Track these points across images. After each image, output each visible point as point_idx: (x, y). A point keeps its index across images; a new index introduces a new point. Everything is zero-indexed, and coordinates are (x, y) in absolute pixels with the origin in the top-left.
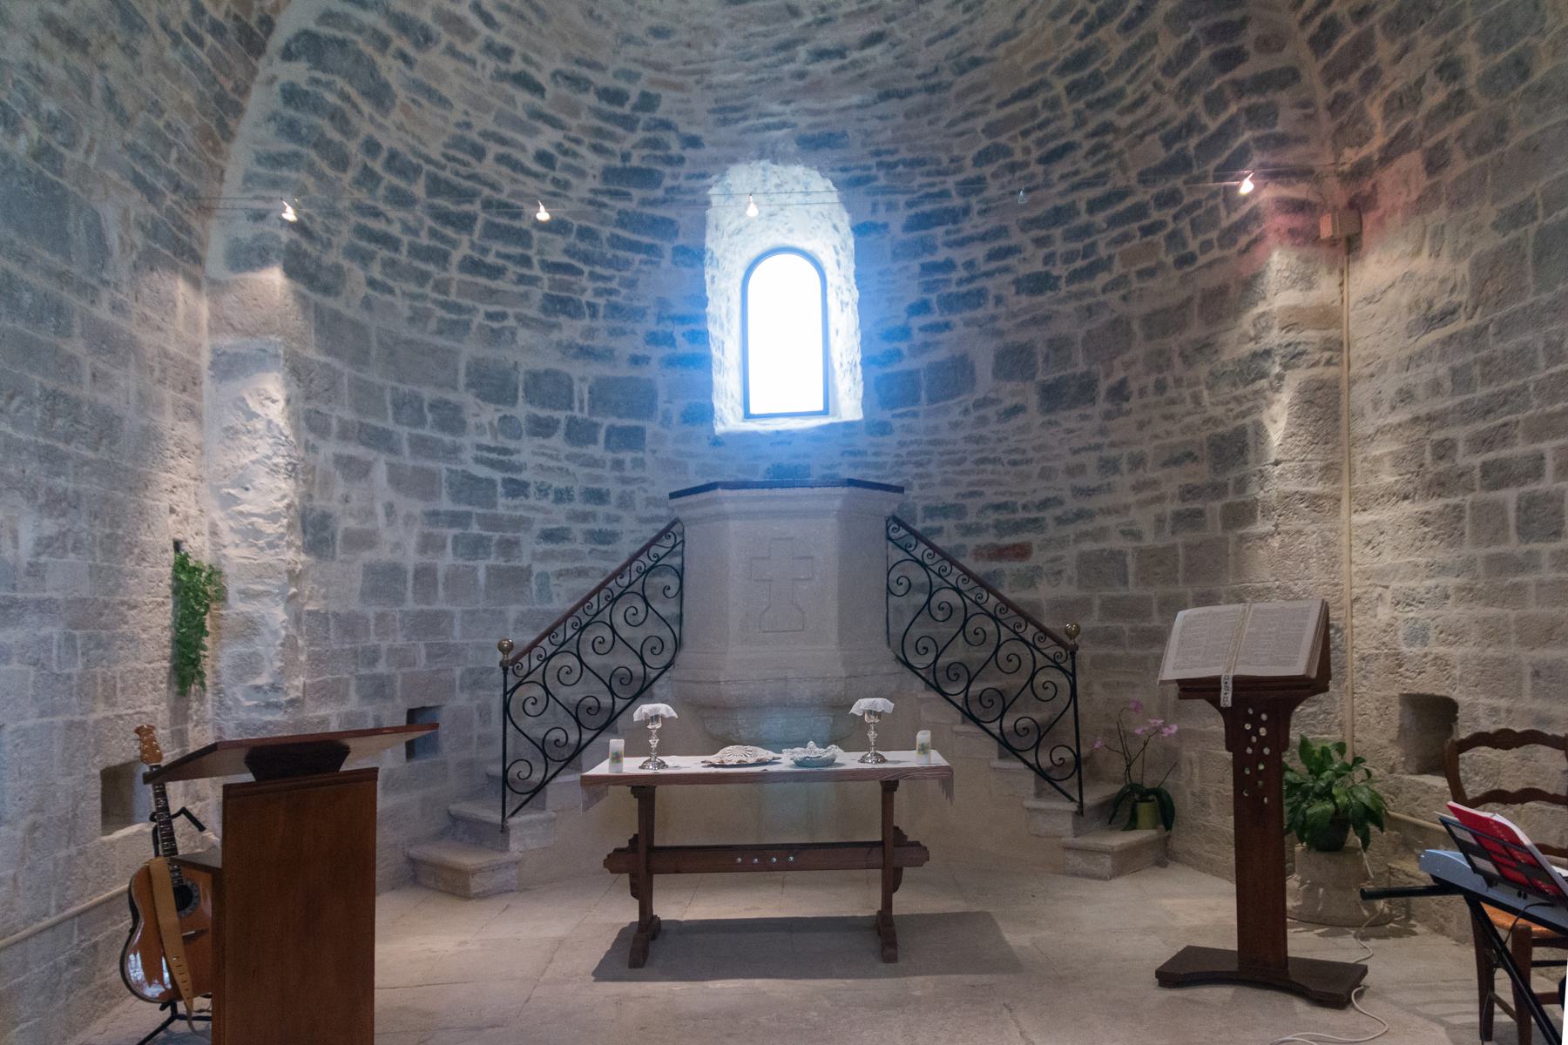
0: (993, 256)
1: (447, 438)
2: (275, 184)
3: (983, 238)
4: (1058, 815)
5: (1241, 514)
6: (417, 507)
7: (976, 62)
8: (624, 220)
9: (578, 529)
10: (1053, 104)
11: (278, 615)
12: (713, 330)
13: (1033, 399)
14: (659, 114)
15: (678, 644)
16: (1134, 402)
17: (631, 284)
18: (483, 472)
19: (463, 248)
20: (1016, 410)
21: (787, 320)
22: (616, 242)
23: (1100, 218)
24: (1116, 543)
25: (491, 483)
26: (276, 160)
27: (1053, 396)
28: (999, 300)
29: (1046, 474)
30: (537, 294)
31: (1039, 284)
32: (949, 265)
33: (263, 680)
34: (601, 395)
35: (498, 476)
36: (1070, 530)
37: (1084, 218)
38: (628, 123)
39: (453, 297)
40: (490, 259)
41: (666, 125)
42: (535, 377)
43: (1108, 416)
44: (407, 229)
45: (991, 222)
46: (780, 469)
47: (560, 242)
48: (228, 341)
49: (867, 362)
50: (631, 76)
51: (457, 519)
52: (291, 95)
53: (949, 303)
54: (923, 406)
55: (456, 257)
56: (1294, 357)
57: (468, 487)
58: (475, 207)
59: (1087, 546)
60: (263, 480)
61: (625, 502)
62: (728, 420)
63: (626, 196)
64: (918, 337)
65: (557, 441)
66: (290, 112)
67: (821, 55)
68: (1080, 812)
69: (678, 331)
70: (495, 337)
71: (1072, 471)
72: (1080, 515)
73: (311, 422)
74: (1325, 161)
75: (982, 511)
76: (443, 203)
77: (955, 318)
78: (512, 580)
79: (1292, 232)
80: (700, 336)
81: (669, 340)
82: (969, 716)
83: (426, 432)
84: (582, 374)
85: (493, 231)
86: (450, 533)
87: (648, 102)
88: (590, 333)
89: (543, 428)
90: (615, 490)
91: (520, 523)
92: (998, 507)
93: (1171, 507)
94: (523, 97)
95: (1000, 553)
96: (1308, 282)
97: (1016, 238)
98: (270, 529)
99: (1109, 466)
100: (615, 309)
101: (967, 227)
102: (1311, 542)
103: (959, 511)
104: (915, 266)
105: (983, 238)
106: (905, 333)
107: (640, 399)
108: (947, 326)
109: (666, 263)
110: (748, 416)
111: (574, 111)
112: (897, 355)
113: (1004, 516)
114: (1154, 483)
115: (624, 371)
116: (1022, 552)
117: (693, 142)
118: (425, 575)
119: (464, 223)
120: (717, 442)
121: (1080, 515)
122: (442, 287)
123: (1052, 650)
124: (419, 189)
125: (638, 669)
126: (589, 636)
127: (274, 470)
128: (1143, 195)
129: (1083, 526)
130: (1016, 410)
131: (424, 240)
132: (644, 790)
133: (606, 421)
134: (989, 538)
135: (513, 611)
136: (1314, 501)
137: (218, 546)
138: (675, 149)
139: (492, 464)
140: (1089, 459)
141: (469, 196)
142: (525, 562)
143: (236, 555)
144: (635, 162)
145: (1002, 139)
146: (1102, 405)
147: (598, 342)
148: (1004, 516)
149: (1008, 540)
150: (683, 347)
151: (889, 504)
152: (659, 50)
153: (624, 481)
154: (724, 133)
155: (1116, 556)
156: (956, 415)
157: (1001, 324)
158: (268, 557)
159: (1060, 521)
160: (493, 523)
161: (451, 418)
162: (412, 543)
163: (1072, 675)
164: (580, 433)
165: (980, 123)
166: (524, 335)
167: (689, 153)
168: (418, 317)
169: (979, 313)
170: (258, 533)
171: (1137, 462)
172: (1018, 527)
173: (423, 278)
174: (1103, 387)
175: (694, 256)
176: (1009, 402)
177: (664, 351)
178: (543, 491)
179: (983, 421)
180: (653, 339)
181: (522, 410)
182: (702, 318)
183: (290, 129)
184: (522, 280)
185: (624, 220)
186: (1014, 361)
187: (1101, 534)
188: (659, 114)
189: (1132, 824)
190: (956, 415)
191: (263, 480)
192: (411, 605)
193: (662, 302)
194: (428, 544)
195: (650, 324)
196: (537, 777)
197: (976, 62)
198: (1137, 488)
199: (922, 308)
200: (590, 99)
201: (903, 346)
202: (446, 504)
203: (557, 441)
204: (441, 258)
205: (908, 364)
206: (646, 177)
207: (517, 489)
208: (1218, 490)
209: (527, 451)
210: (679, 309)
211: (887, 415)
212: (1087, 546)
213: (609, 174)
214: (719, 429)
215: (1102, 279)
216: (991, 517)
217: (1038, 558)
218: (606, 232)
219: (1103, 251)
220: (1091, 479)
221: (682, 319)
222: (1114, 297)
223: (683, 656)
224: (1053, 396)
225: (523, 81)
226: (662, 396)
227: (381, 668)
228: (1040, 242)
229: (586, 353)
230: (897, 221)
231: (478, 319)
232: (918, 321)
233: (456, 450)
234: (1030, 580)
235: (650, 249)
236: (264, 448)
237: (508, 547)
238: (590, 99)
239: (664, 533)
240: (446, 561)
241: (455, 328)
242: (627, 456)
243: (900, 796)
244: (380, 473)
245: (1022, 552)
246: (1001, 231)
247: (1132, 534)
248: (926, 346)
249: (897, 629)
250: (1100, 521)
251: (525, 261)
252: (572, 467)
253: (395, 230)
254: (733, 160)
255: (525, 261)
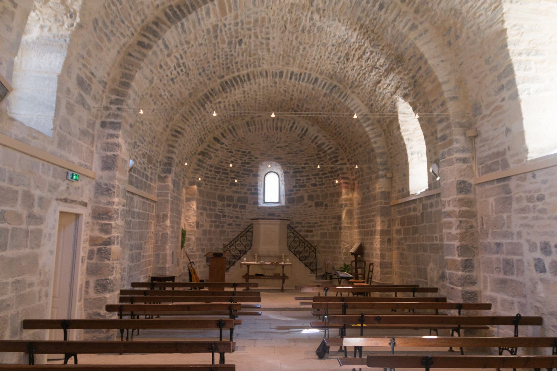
0: (307, 179)
1: (214, 208)
2: (196, 173)
3: (306, 176)
4: (313, 277)
5: (340, 228)
6: (209, 220)
7: (303, 151)
8: (244, 170)
9: (234, 223)
10: (315, 159)
11: (193, 238)
12: (259, 188)
13: (314, 205)
14: (251, 154)
15: (251, 245)
16: (328, 208)
17: (245, 180)
18: (219, 213)
19: (218, 177)
20: (311, 206)
21: (272, 188)
22: (243, 174)
23: (323, 176)
24: (326, 231)
25: (220, 215)
26: (196, 170)
27: (317, 204)
28: (308, 187)
29: (316, 218)
30: (229, 183)
31: (314, 185)
32: (300, 180)
33: (191, 248)
34: (239, 200)
35: (221, 214)
36: (319, 228)
37: (321, 176)
38: (246, 156)
39: (216, 184)
40: (222, 178)
41: (252, 156)
42: (228, 197)
43: (325, 209)
44: (211, 175)
45: (307, 174)
46: (271, 213)
47: (233, 174)
48: (188, 196)
49: (286, 195)
50: (247, 149)
51: (215, 222)
52: (199, 160)
53: (300, 186)
54: (295, 204)
55: (217, 178)
56: (346, 205)
57: (217, 216)
58: (221, 170)
59: (322, 231)
60: (192, 217)
61: (242, 219)
62: (261, 204)
63: (245, 166)
64: (295, 192)
65: (231, 208)
66: (199, 163)
67: (278, 147)
68: (316, 276)
69: (252, 188)
70: (222, 190)
71: (320, 218)
72: (321, 226)
73: (198, 207)
74: (350, 177)
75: (305, 223)
76: (216, 170)
77: (301, 189)
78: (222, 232)
79: (346, 187)
80: (256, 189)
81: (251, 190)
82: (300, 260)
83: (211, 207)
84: (236, 196)
85: (223, 173)
86: (214, 224)
87: (249, 153)
88: (237, 189)
89: (229, 205)
90: (240, 216)
91: (225, 222)
92: (308, 223)
93: (333, 226)
94: (230, 154)
95: (308, 231)
96: (348, 194)
97: (311, 177)
98: (193, 225)
99: (325, 218)
100: (242, 185)
101: (303, 174)
102: (348, 234)
103: (302, 223)
104: (294, 179)
105: (306, 176)
106: (292, 191)
107: (246, 200)
108: (300, 190)
109: (251, 177)
110: (264, 203)
111: (238, 155)
112: (291, 194)
113: (309, 225)
114: (331, 222)
115: (243, 195)
116: (311, 231)
117: (257, 158)
118: (210, 231)
119: (219, 172)
120: (259, 208)
121: (321, 226)
122: (215, 183)
123: (313, 249)
124: (213, 169)
125: (245, 249)
126: (237, 243)
127: (194, 216)
128: (329, 175)
129: (321, 228)
130: (311, 206)
131: (213, 176)
132: (248, 266)
133: (239, 204)
134: (306, 229)
135: (223, 238)
136: (349, 227)
137: (185, 227)
138: (253, 159)
139: (220, 212)
140: (322, 216)
141: (220, 169)
142: (225, 229)
143: (188, 228)
144: (247, 161)
145: (308, 162)
146: (324, 207)
147: (239, 190)
148: (309, 225)
149: (309, 229)
150: (253, 191)
151: (288, 223)
152: (252, 146)
153: (242, 215)
154: (261, 157)
155: (326, 233)
156: (301, 206)
157: (309, 191)
158: (192, 229)
159: (318, 226)
160: (220, 222)
161: (215, 205)
162: (208, 226)
163: (315, 253)
164: (235, 206)
165: (304, 159)
166: (227, 190)
167: (256, 160)
168: (211, 188)
169: (305, 189)
170: (191, 225)
171: (329, 218)
172: (311, 227)
173: (212, 182)
174: (324, 204)
175: (256, 176)
176: (310, 205)
177: (250, 192)
178: (228, 217)
179: (305, 207)
180: (248, 190)
181: (226, 202)
182: (257, 186)
183: (199, 165)
184: (227, 181)
185: (244, 170)
186: (310, 198)
187: (323, 229)
188: (251, 154)
189: (326, 279)
190: (301, 206)
191: (192, 217)
192: (208, 237)
193: (250, 183)
194: (211, 226)
195: (248, 187)
196: (228, 267)
197: (303, 151)
198: (329, 222)
199: (295, 187)
200: (240, 153)
201: (292, 193)
202: (213, 219)
203: (231, 208)
204: (215, 178)
205: (293, 196)
206: (248, 163)
207: (224, 216)
208: (338, 224)
209: (226, 210)
210: (253, 184)
211: (289, 205)
212: (322, 231)
213: (242, 163)
214: (259, 205)
215: (324, 186)
216: (307, 225)
217: (314, 233)
218: (241, 172)
219: (324, 182)
220: (322, 220)
221: (253, 186)
222: (325, 189)
223: (252, 247)
224: (317, 204)
225: (231, 152)
226: (249, 199)
227: (204, 247)
228: (315, 178)
229: (236, 192)
230: (291, 171)
231: (220, 187)
232: (295, 189)
233: (215, 210)
234: (313, 236)
235: (248, 174)
236: (192, 212)
237: (223, 226)
238: (240, 153)
239: (250, 226)
240: (213, 229)
241: (216, 189)
242: (243, 210)
243: (284, 268)
244: (205, 214)
245: (311, 231)
246: (308, 176)
247: (328, 230)
248: (296, 193)
249: (289, 244)
250: (324, 227)
251: (228, 177)
252: (233, 212)
253: (209, 175)
254: (263, 161)
255: (228, 177)
